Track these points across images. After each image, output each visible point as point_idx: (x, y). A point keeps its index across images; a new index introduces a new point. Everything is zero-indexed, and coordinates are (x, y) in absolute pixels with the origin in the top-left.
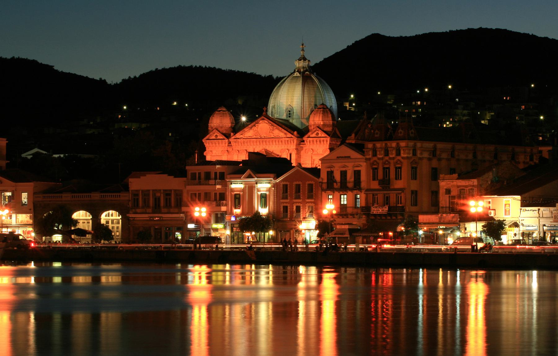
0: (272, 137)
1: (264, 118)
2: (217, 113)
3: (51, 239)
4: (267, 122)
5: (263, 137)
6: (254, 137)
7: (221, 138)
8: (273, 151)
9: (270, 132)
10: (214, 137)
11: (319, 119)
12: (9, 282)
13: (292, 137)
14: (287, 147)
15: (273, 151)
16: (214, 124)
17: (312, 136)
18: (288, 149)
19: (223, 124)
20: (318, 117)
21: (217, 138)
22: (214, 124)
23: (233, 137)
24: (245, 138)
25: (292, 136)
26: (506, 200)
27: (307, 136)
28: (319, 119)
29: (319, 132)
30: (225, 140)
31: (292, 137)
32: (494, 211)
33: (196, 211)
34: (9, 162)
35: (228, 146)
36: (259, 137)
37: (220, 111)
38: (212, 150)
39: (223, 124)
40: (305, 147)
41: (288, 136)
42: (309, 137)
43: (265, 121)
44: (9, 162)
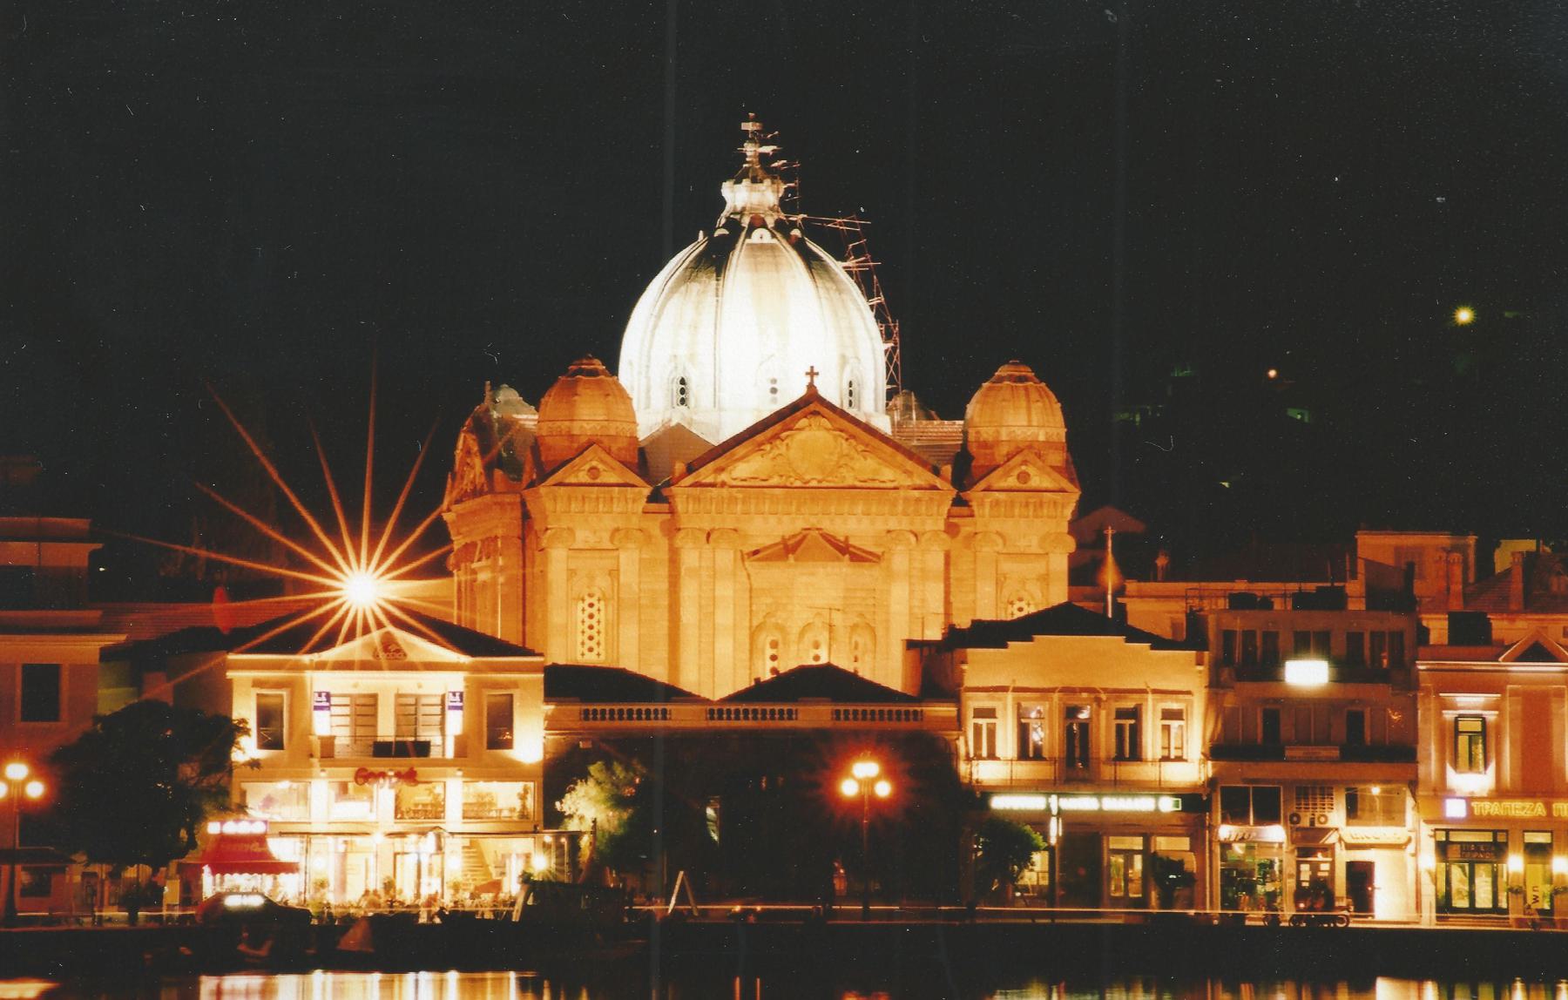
0: (850, 482)
1: (817, 409)
2: (585, 382)
3: (1378, 797)
4: (829, 425)
5: (814, 483)
6: (775, 481)
7: (613, 479)
8: (847, 538)
9: (838, 462)
10: (583, 477)
11: (1030, 421)
12: (1035, 985)
13: (934, 488)
14: (912, 523)
15: (847, 538)
16: (585, 425)
17: (997, 485)
18: (912, 532)
19: (1013, 429)
20: (1023, 412)
21: (598, 481)
22: (585, 425)
23: (689, 480)
24: (734, 483)
25: (938, 482)
26: (265, 882)
27: (982, 484)
28: (1030, 421)
29: (1031, 470)
30: (636, 489)
31: (934, 488)
32: (1451, 833)
33: (853, 777)
34: (99, 546)
35: (645, 513)
36: (798, 483)
37: (1001, 380)
38: (571, 525)
39: (1013, 429)
40: (965, 526)
41: (918, 482)
42: (988, 489)
43: (823, 420)
44: (99, 546)
